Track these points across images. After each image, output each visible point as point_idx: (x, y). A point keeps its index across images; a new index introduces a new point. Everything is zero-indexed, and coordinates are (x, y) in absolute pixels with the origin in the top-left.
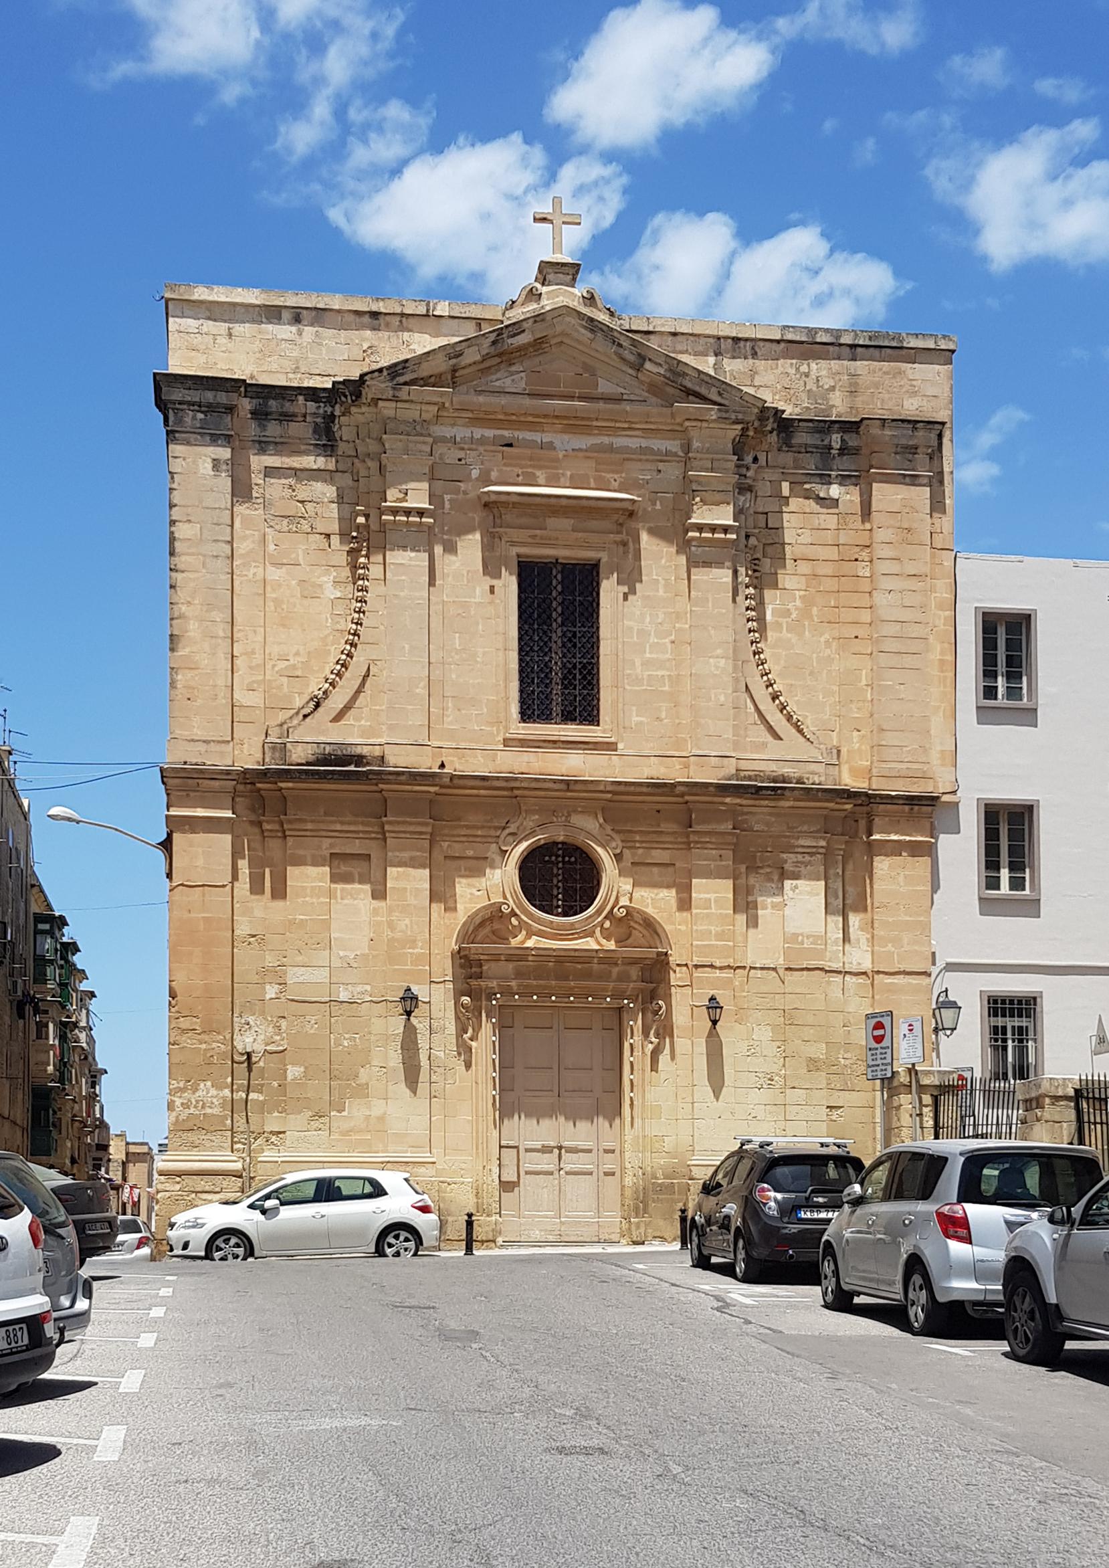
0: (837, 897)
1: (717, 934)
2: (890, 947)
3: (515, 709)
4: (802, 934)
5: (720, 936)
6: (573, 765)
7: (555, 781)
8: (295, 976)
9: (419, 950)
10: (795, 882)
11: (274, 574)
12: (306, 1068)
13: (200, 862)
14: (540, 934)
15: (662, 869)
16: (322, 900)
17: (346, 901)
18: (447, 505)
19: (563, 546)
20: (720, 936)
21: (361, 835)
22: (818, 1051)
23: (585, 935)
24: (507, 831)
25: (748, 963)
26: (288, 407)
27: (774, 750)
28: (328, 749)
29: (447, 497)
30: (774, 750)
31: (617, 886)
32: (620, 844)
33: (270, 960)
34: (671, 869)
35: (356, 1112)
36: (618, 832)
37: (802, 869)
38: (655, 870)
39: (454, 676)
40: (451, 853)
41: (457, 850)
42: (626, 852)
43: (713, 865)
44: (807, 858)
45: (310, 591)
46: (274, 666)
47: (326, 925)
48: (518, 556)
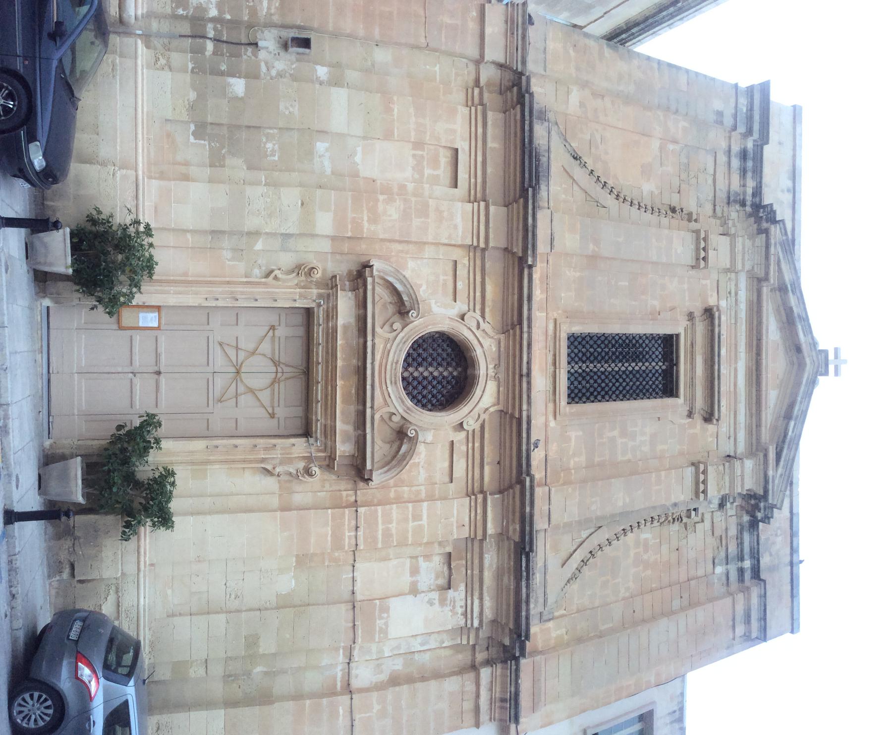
0: (422, 644)
1: (388, 529)
2: (377, 707)
3: (577, 329)
4: (388, 616)
5: (387, 534)
6: (540, 382)
7: (529, 363)
8: (339, 97)
9: (366, 224)
10: (437, 602)
11: (656, 144)
12: (242, 98)
13: (447, 20)
14: (390, 348)
15: (447, 470)
16: (413, 134)
17: (411, 159)
18: (704, 282)
19: (690, 369)
20: (387, 534)
21: (473, 180)
22: (267, 646)
23: (390, 398)
24: (481, 320)
25: (357, 565)
26: (749, 174)
27: (553, 562)
28: (544, 160)
29: (708, 281)
30: (553, 562)
31: (436, 430)
32: (470, 429)
33: (352, 75)
34: (447, 479)
35: (194, 150)
36: (482, 427)
37: (449, 608)
38: (446, 464)
39: (600, 278)
40: (459, 267)
41: (462, 272)
42: (463, 435)
43: (454, 520)
44: (460, 611)
45: (646, 171)
46: (597, 130)
47: (388, 136)
48: (678, 336)
